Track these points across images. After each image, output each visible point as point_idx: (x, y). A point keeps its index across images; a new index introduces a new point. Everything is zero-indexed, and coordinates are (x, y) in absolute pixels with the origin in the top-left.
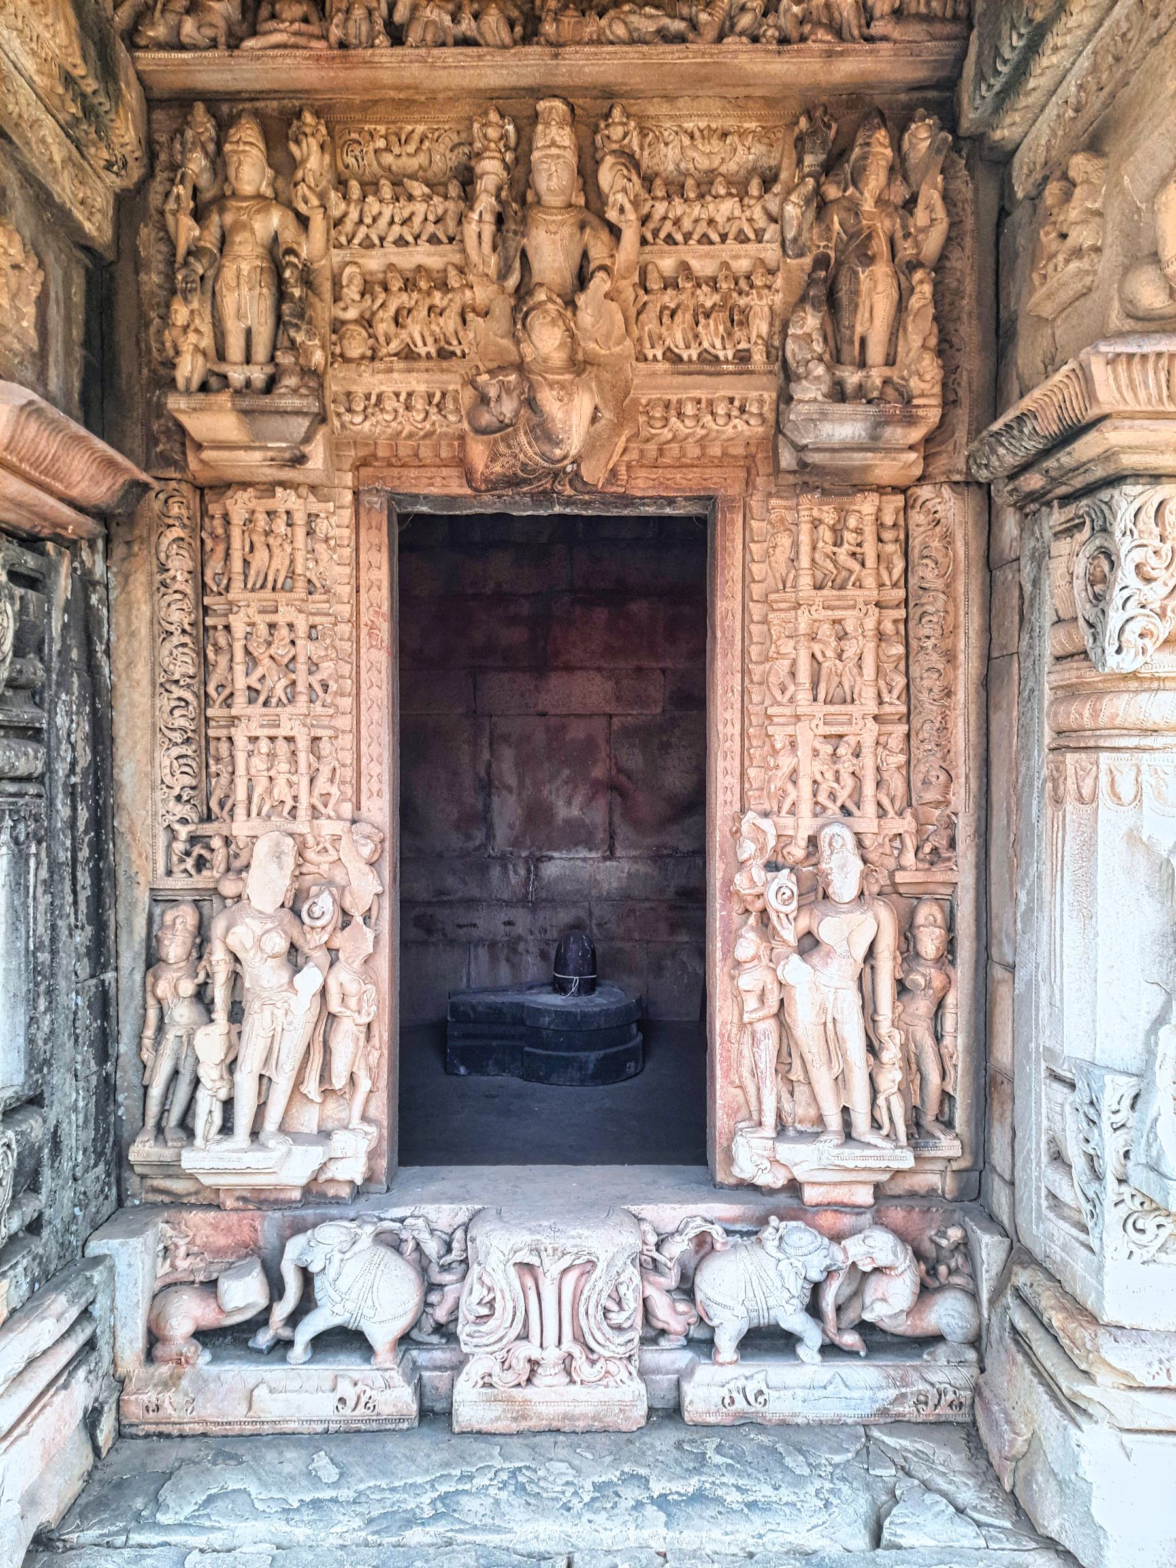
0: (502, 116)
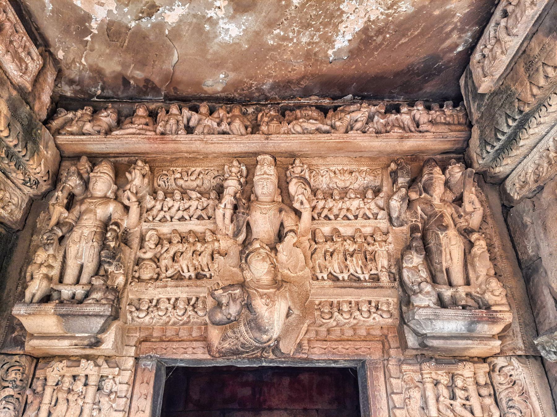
0: (240, 164)
